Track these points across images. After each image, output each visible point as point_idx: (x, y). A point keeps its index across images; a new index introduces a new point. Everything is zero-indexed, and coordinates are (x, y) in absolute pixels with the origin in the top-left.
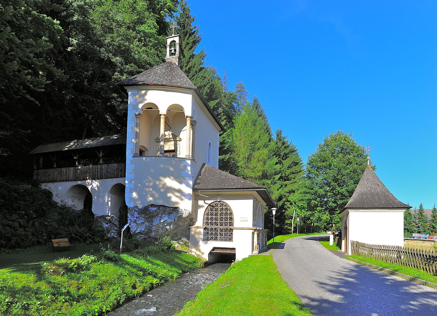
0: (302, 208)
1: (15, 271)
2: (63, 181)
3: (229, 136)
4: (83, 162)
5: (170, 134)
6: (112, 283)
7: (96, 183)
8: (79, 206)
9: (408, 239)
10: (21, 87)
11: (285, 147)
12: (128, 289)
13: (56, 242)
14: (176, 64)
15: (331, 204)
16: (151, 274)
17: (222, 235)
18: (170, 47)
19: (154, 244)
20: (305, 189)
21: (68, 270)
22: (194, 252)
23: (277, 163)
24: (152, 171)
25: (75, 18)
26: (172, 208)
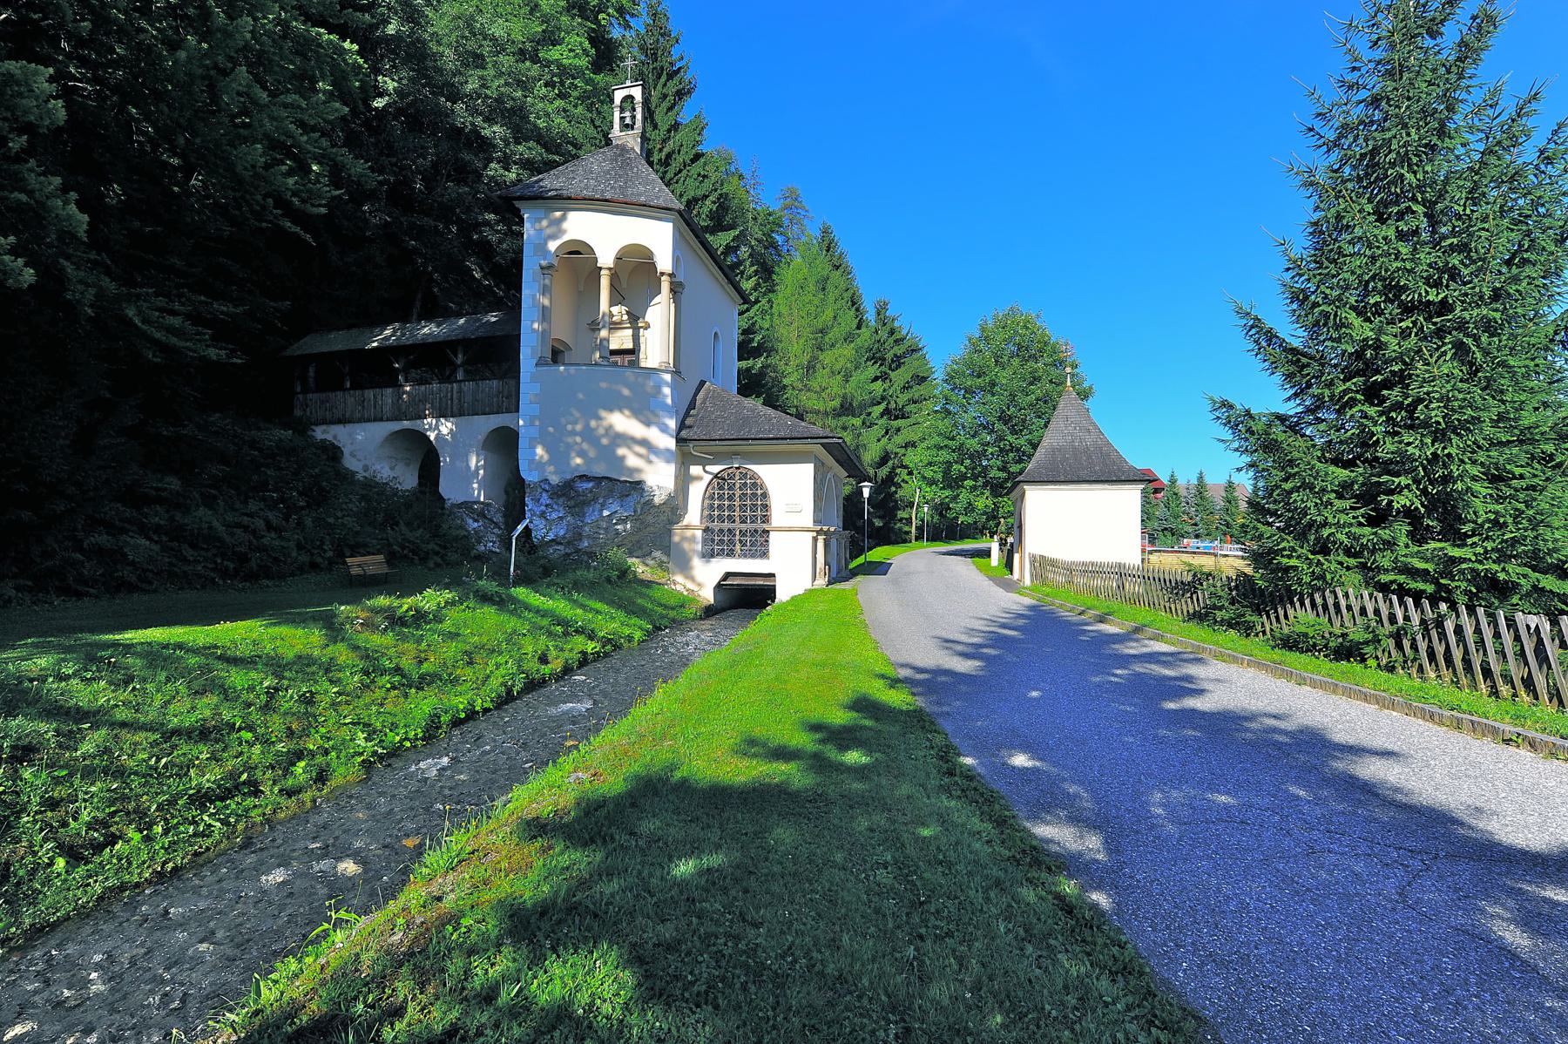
0: (931, 482)
1: (275, 624)
2: (369, 420)
3: (764, 312)
4: (414, 375)
5: (624, 312)
6: (494, 651)
7: (449, 425)
8: (408, 480)
9: (1160, 551)
10: (270, 201)
11: (896, 341)
12: (531, 664)
13: (357, 564)
14: (635, 151)
15: (994, 473)
16: (583, 633)
17: (745, 545)
18: (622, 110)
19: (588, 567)
20: (937, 439)
21: (396, 621)
22: (680, 583)
23: (876, 379)
24: (580, 396)
25: (391, 29)
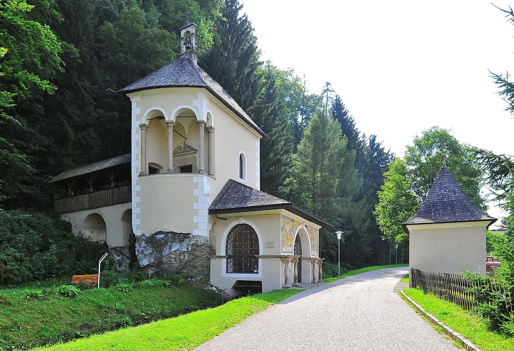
2: (80, 210)
26: (182, 235)
